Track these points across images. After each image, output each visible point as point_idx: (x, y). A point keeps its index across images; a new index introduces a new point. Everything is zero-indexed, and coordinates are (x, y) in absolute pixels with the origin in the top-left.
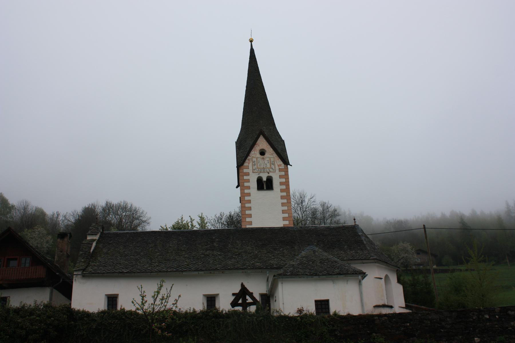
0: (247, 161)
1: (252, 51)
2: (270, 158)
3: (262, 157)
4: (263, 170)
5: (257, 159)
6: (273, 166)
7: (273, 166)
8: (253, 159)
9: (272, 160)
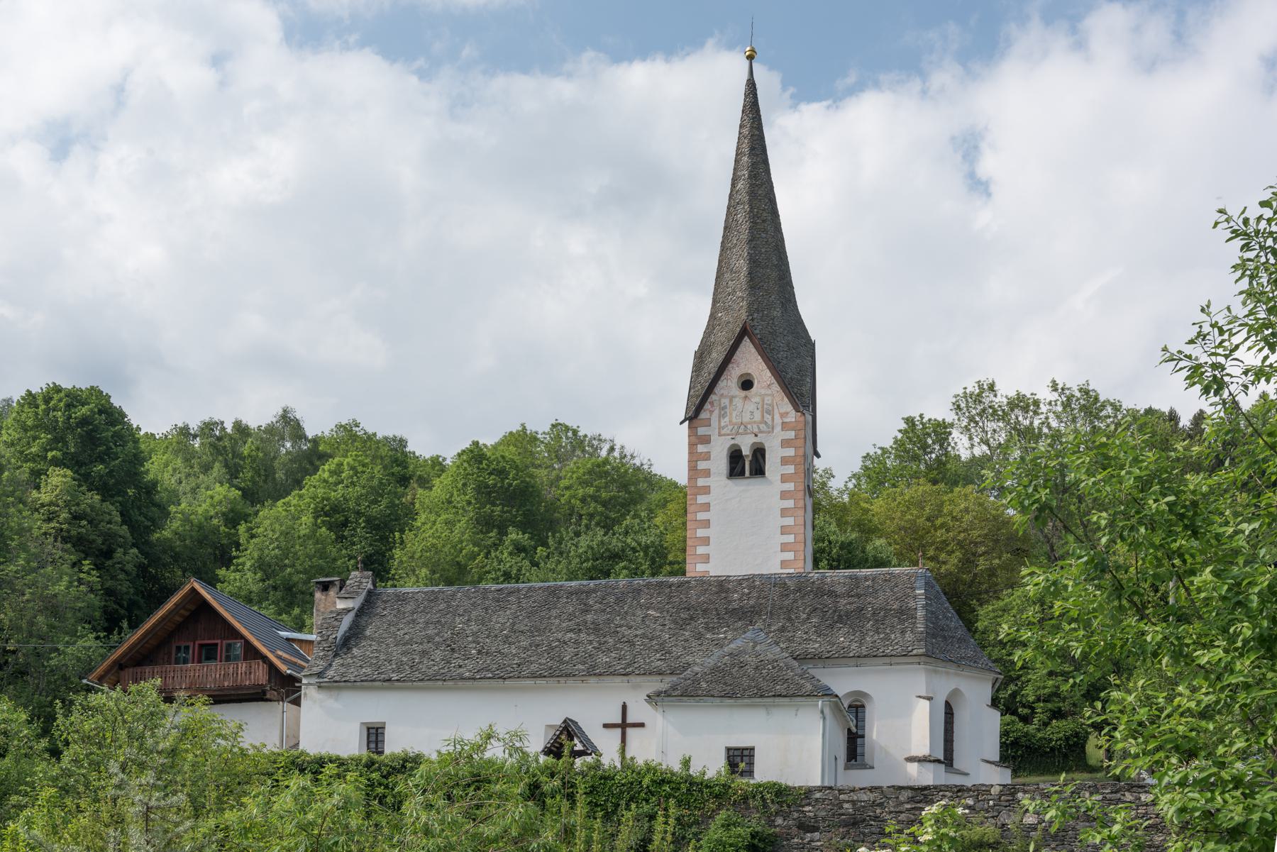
0: (707, 406)
1: (751, 87)
2: (763, 397)
3: (744, 393)
4: (742, 428)
5: (731, 401)
6: (768, 418)
7: (768, 418)
8: (723, 401)
9: (768, 400)
